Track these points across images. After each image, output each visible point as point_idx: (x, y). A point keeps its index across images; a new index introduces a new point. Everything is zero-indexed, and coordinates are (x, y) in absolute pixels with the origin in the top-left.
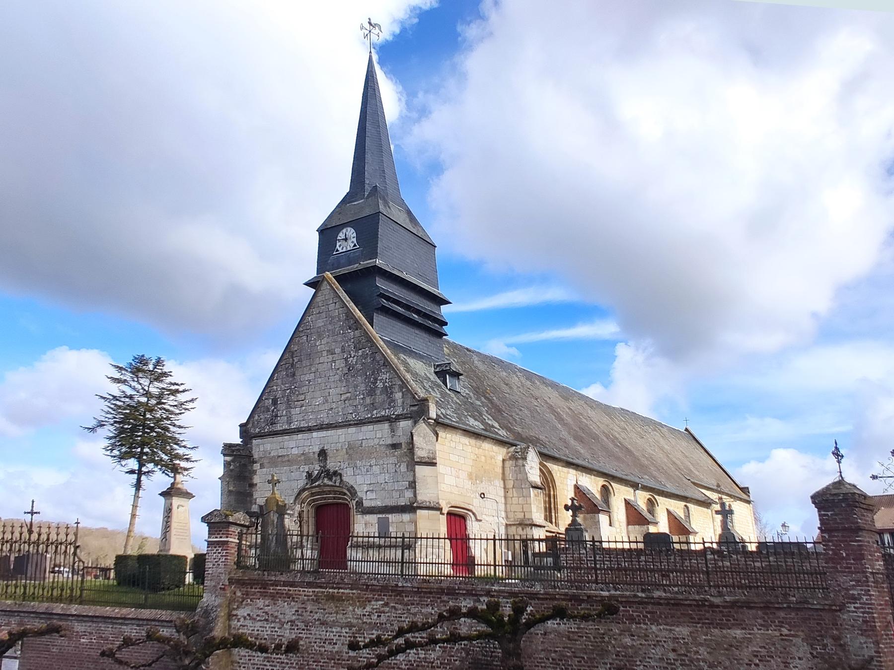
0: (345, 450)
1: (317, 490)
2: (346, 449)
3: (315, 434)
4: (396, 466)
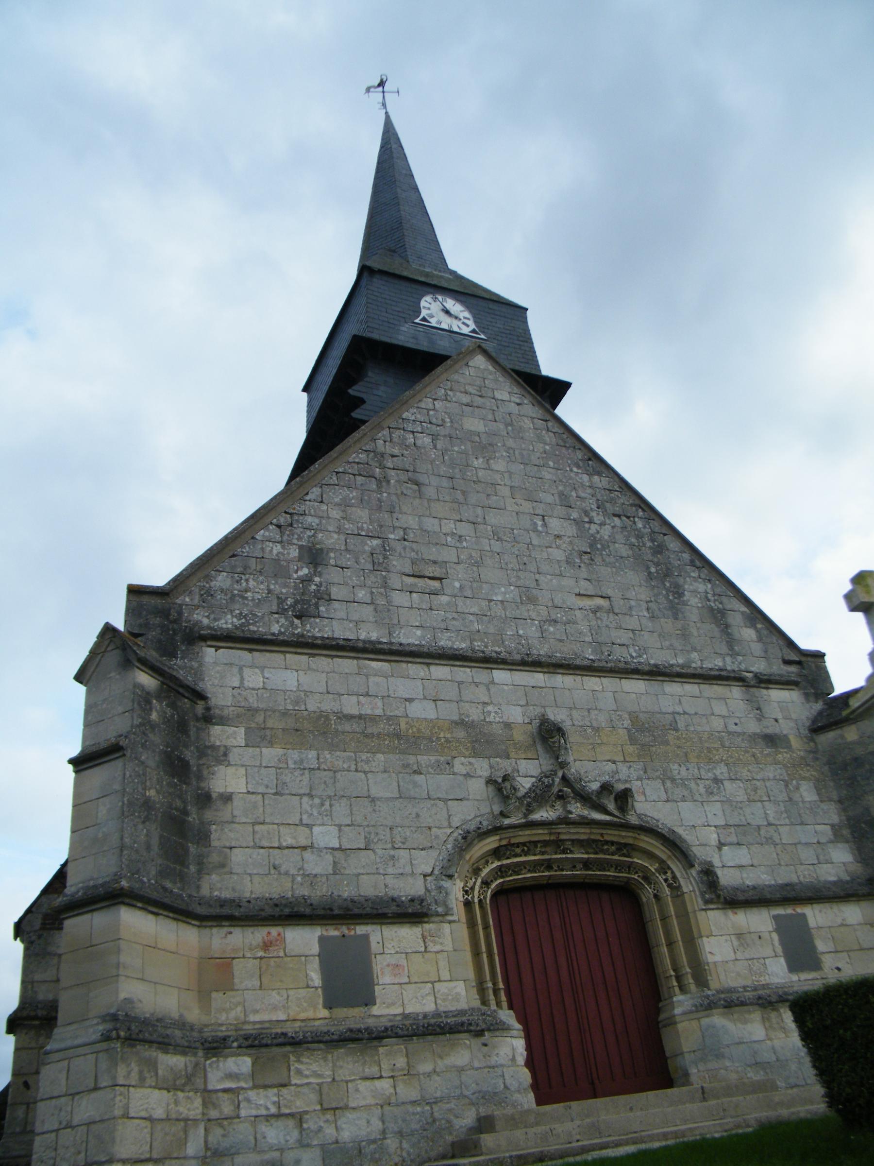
0: (623, 733)
1: (541, 834)
2: (629, 731)
3: (500, 675)
4: (787, 786)
